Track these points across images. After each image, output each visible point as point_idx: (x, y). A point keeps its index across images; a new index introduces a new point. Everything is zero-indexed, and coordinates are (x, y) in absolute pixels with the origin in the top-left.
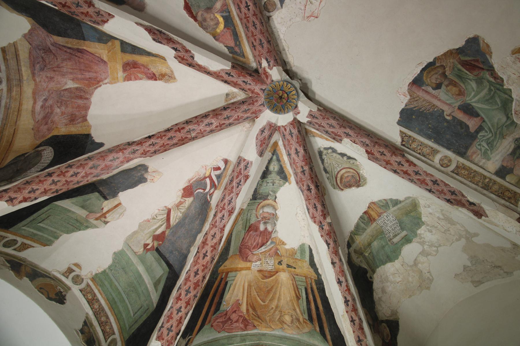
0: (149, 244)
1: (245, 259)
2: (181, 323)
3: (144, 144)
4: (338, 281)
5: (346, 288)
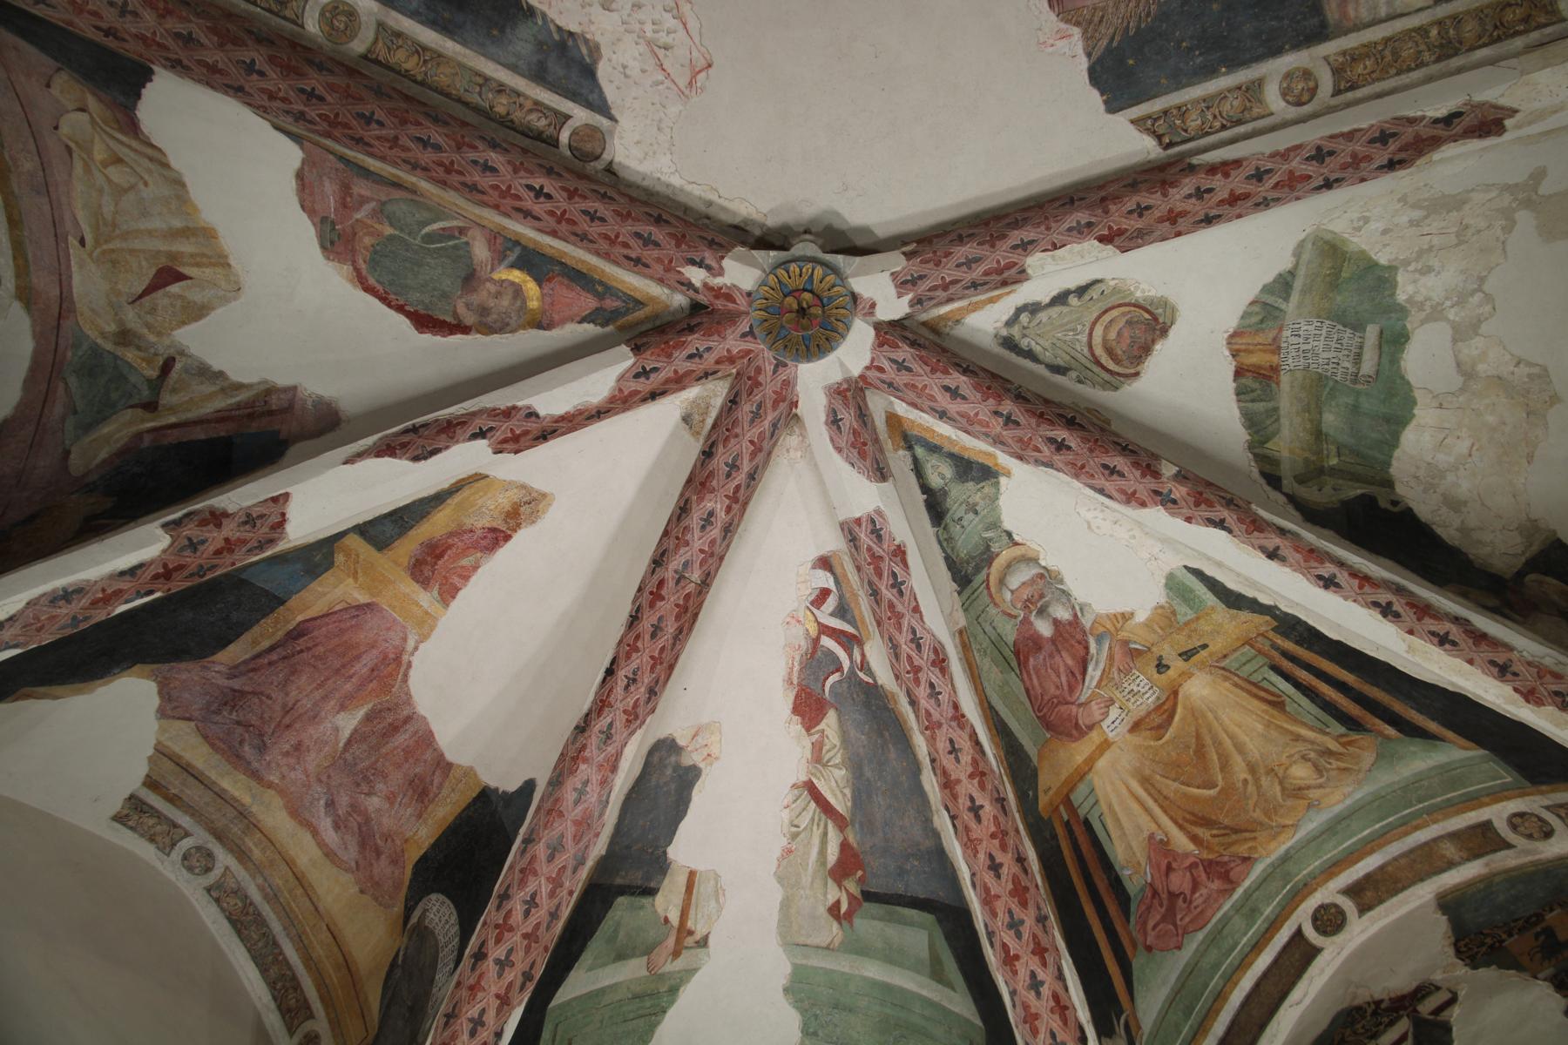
0: (838, 902)
1: (1074, 732)
2: (1066, 1008)
3: (612, 699)
4: (1321, 583)
5: (1356, 582)
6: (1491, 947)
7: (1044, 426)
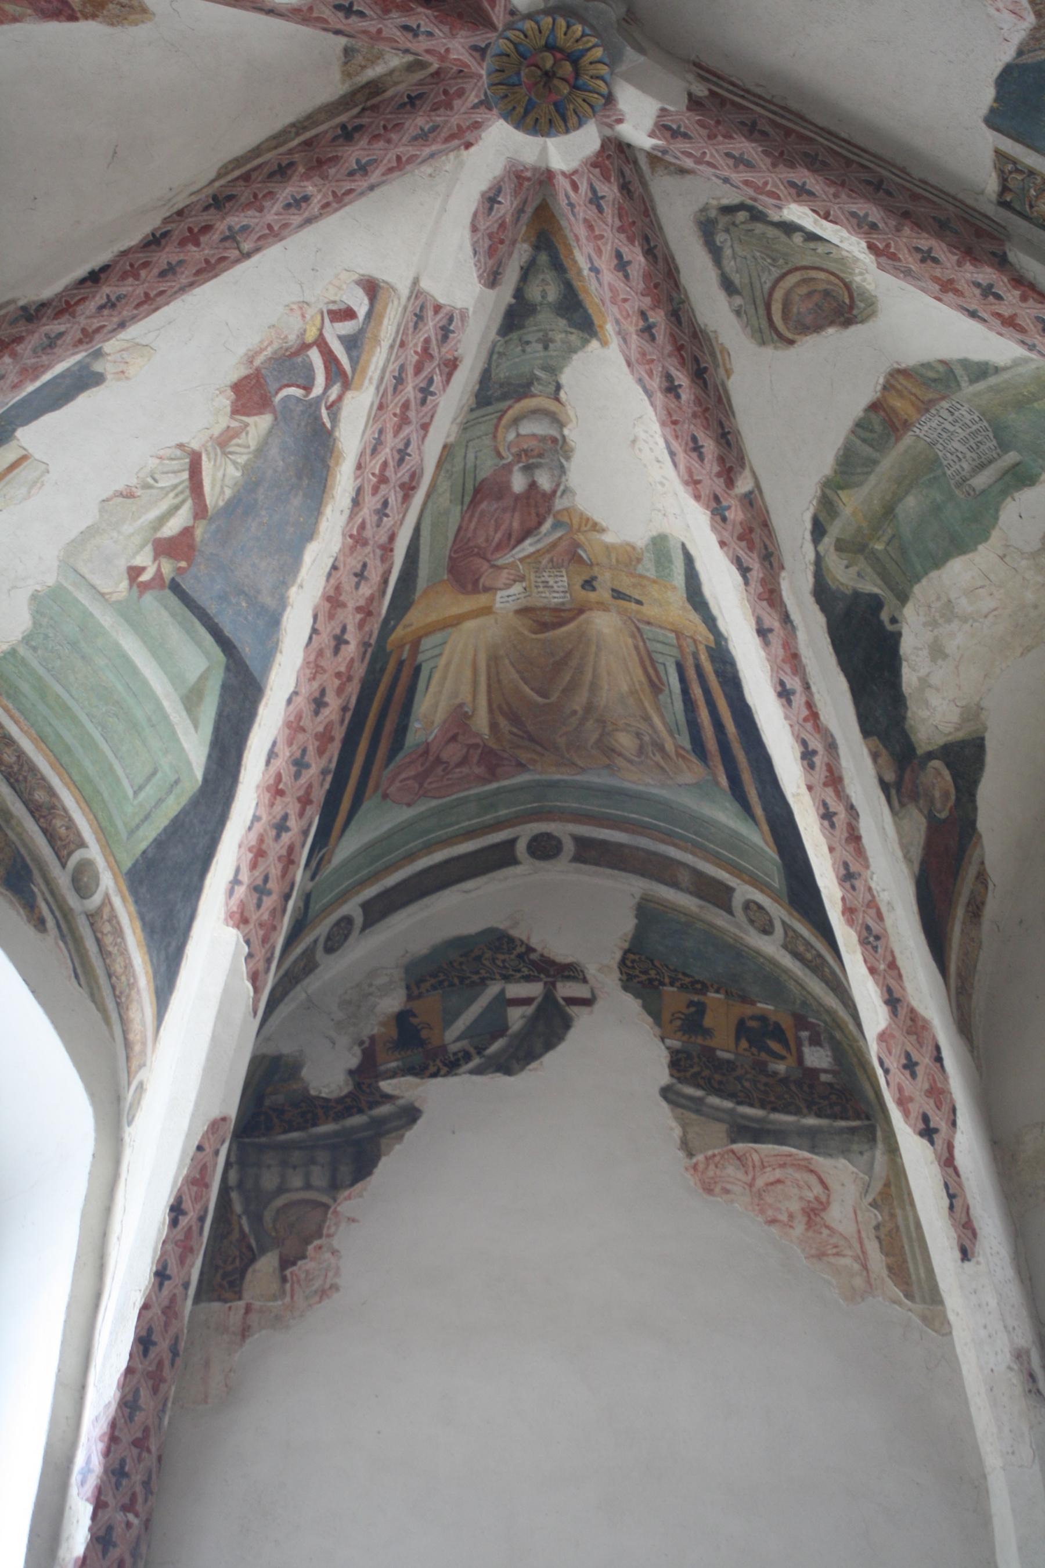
1: (470, 587)
3: (80, 308)
4: (779, 689)
5: (805, 712)
6: (651, 981)
7: (675, 361)
